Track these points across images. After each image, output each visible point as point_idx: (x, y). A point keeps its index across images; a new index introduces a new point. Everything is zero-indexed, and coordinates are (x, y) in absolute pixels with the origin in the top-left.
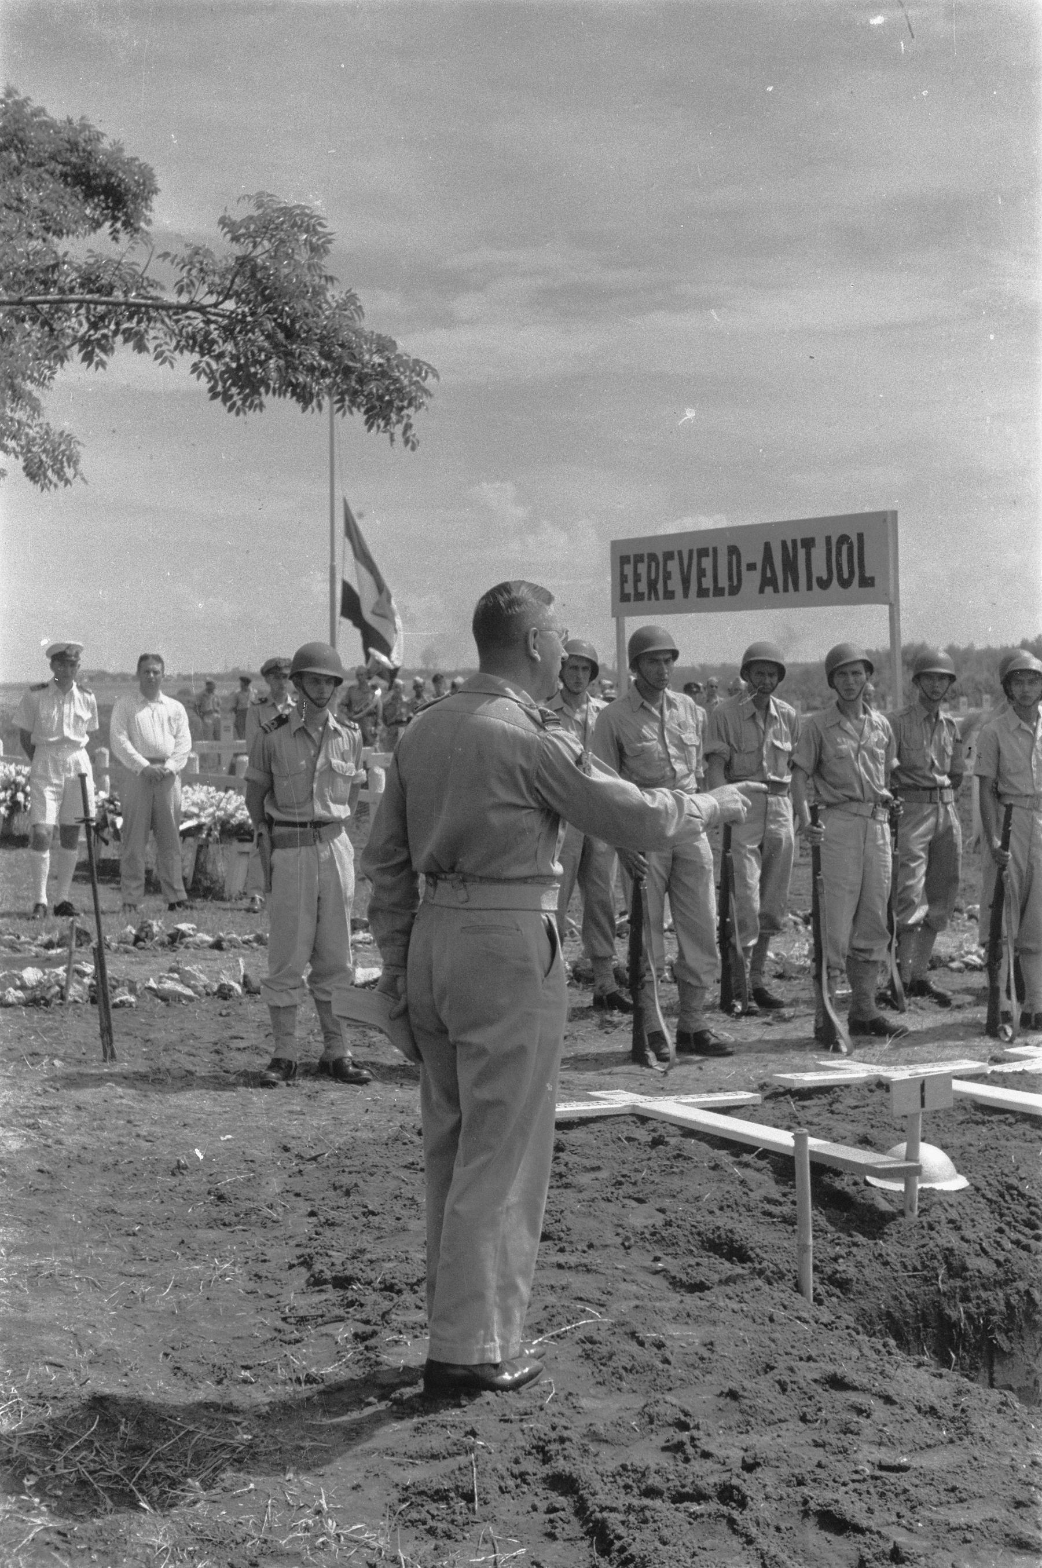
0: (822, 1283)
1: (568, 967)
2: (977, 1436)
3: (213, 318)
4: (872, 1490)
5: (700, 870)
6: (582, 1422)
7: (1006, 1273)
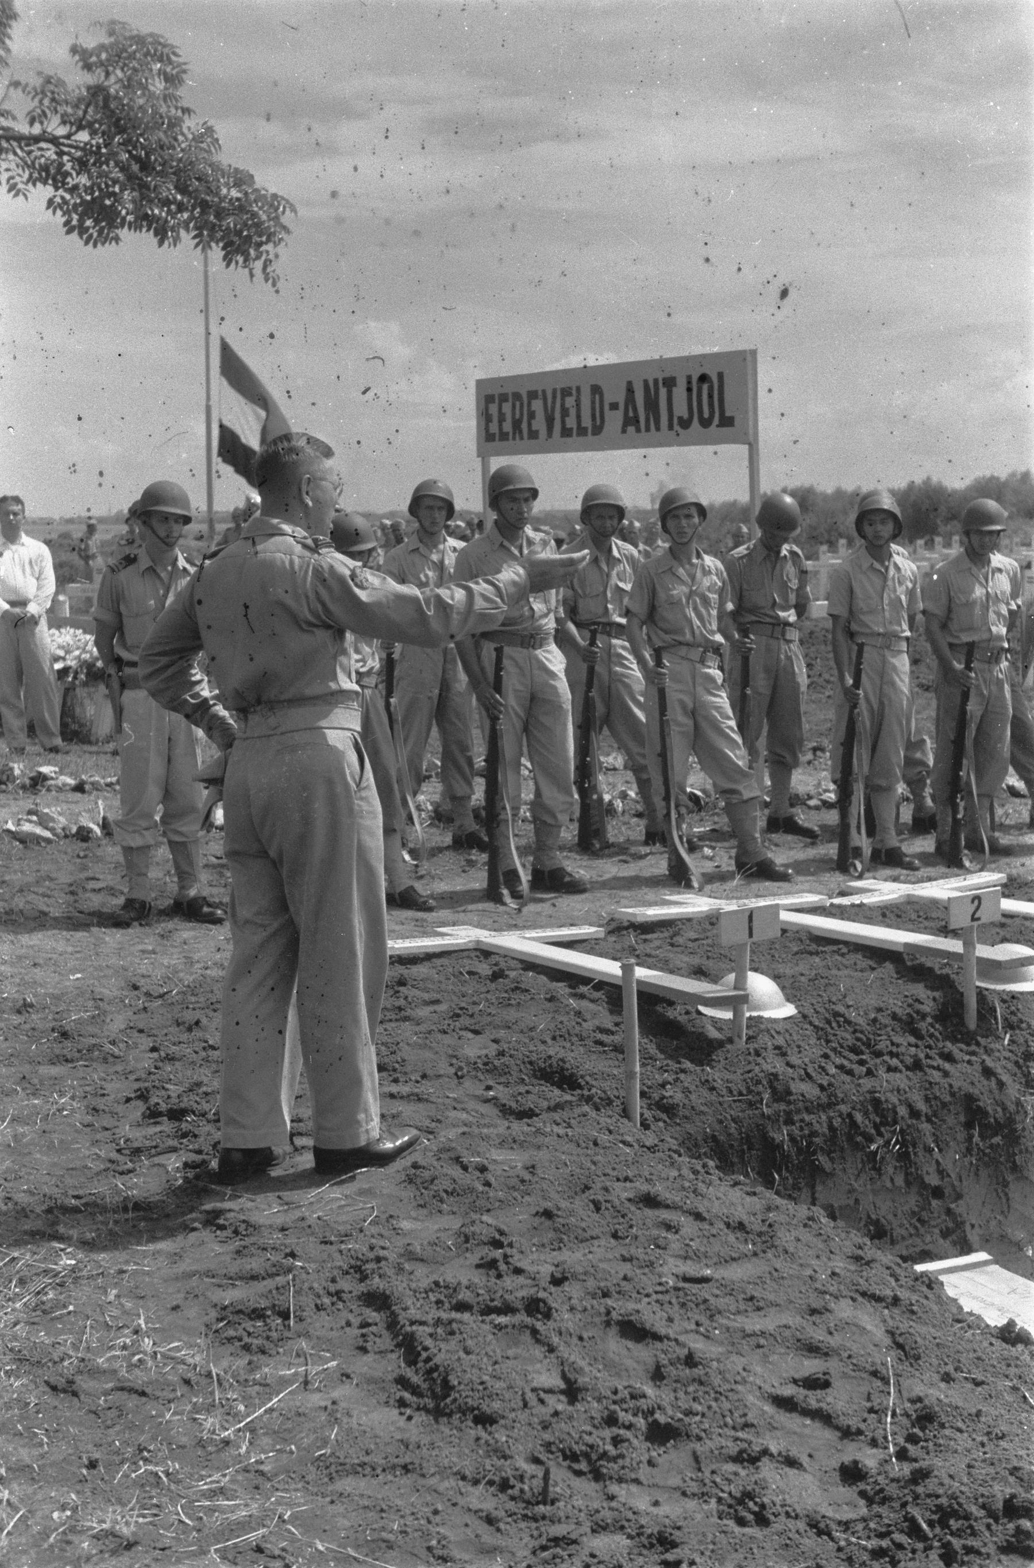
0: (649, 1109)
1: (430, 808)
2: (780, 1249)
3: (66, 149)
4: (674, 1301)
5: (556, 708)
6: (400, 1242)
7: (829, 1097)
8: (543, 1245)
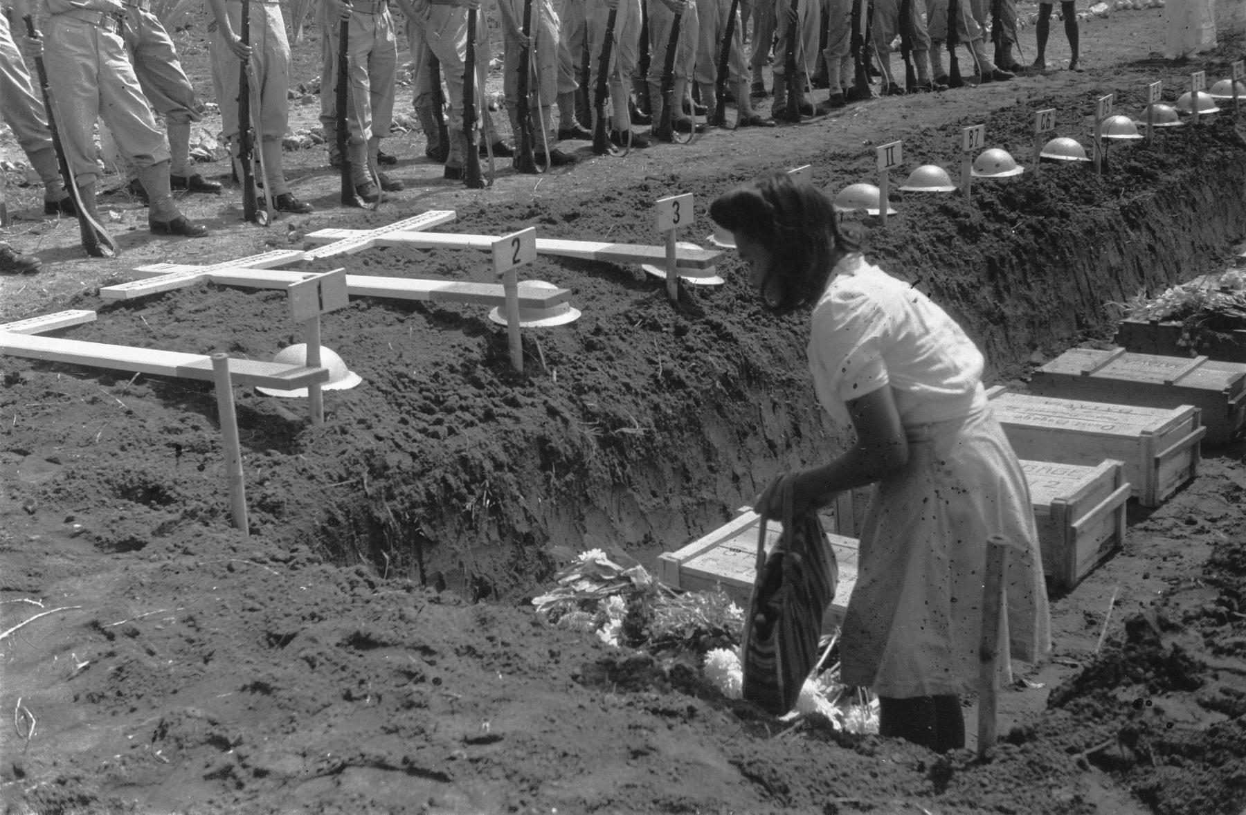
7: (422, 463)
8: (273, 730)
